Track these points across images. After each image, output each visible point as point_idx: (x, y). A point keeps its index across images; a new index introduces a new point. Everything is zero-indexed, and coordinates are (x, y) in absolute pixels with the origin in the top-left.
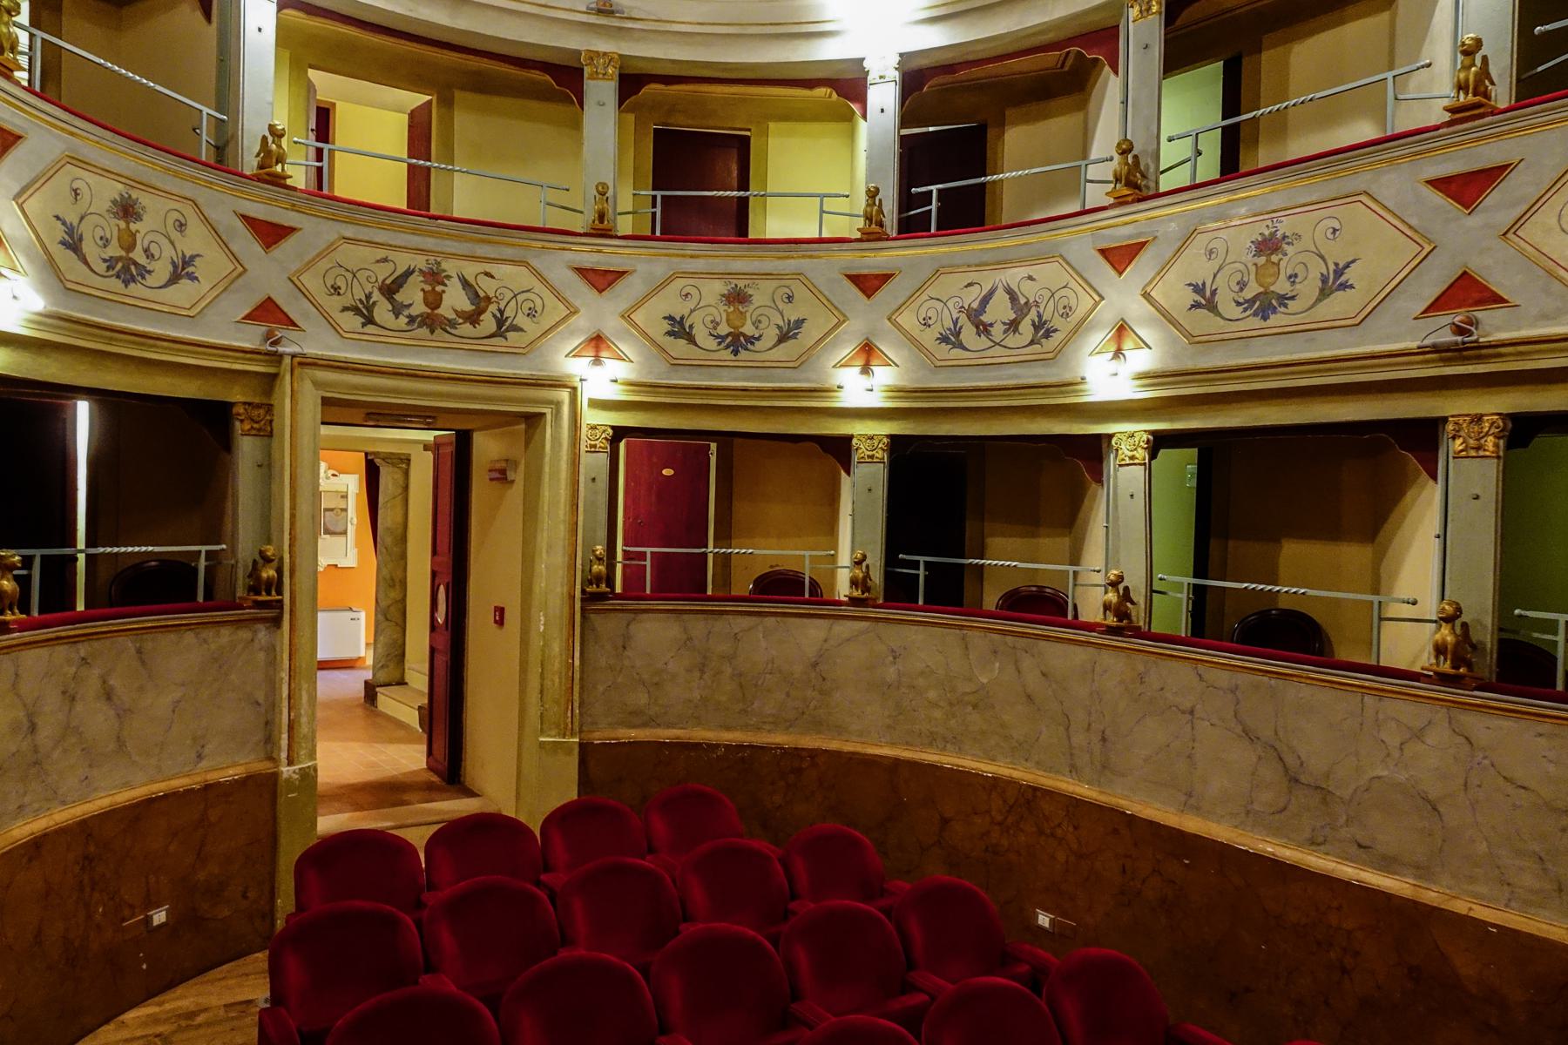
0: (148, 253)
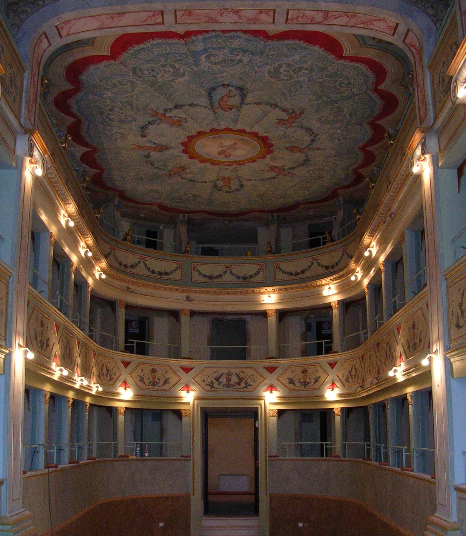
0: (159, 379)
